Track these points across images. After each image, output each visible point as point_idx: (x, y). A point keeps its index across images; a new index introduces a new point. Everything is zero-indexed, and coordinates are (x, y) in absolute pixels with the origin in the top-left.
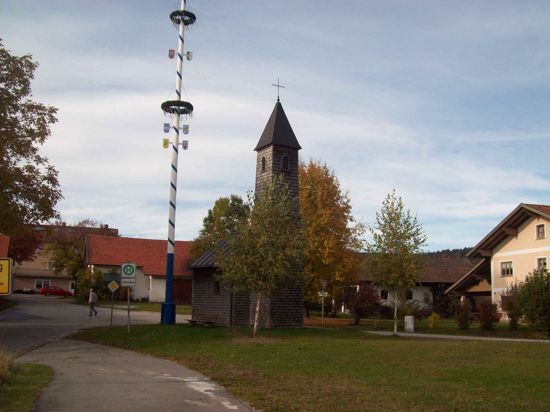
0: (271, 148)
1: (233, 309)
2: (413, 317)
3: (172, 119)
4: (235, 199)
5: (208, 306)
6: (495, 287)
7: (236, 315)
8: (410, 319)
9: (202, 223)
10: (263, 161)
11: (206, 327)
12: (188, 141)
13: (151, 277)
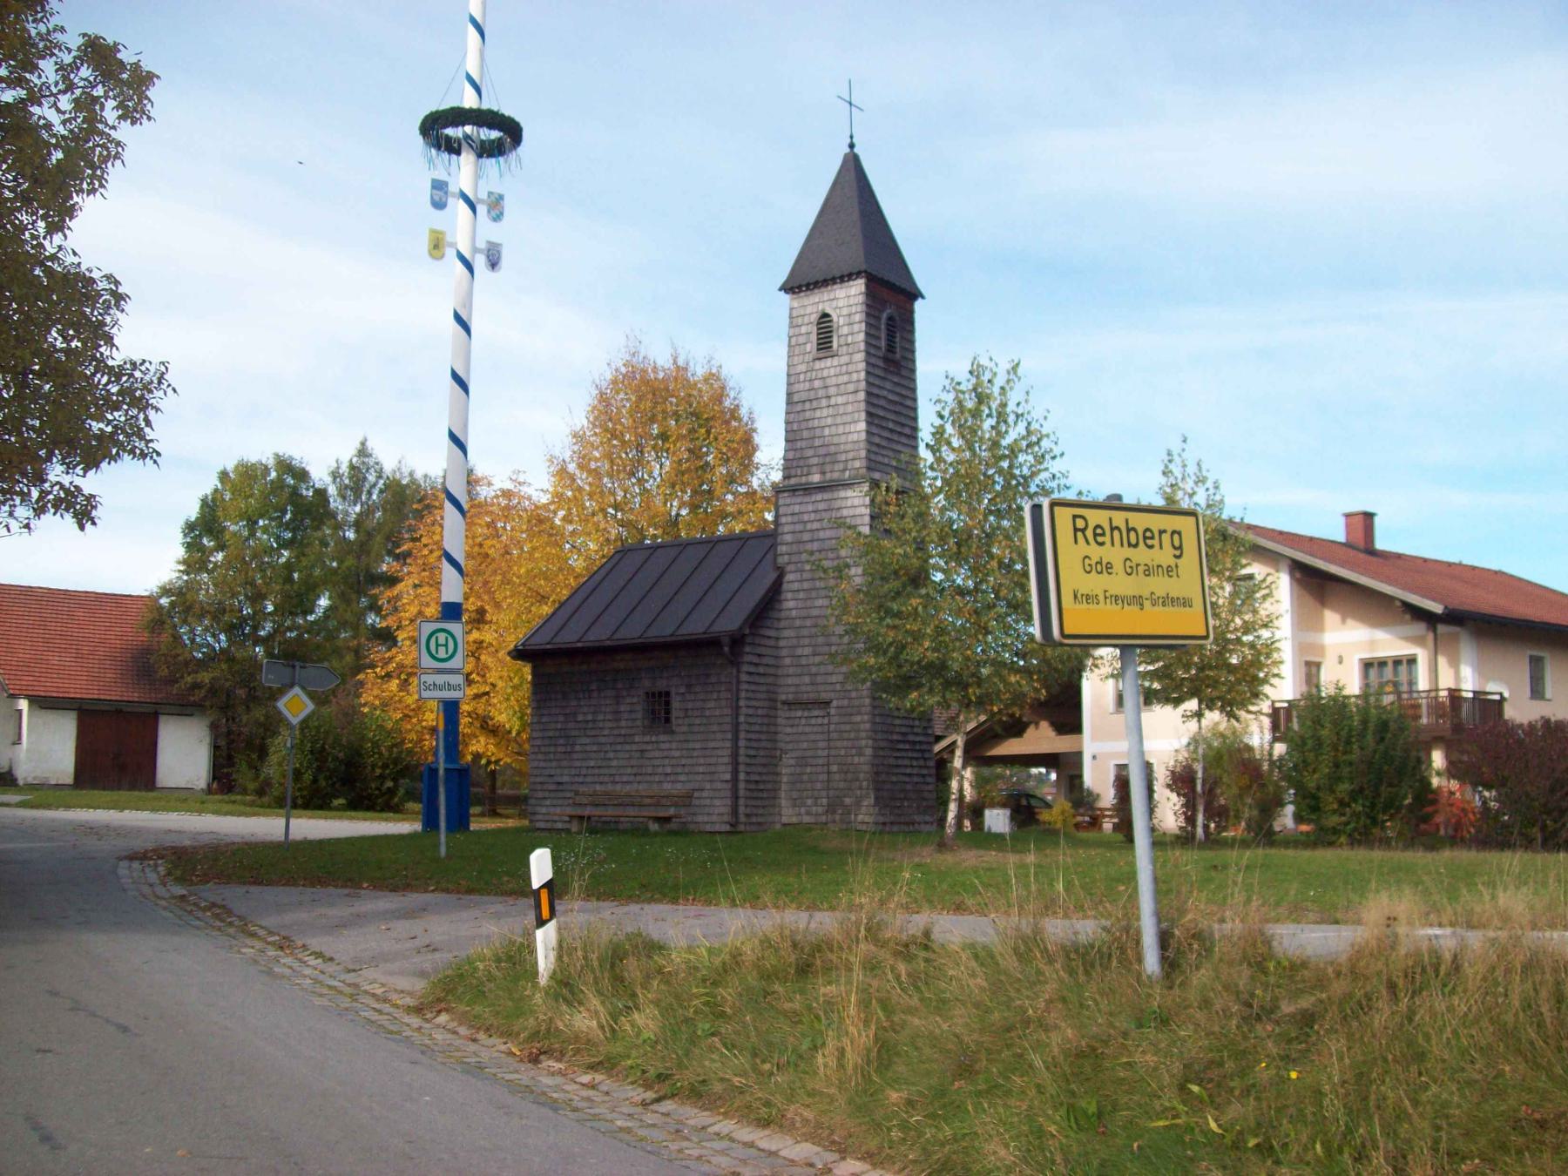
0: (857, 287)
1: (742, 776)
2: (1007, 812)
3: (464, 171)
4: (285, 466)
5: (613, 771)
6: (1094, 738)
7: (748, 794)
8: (1001, 817)
9: (180, 537)
10: (819, 323)
11: (656, 834)
12: (500, 245)
13: (23, 705)
